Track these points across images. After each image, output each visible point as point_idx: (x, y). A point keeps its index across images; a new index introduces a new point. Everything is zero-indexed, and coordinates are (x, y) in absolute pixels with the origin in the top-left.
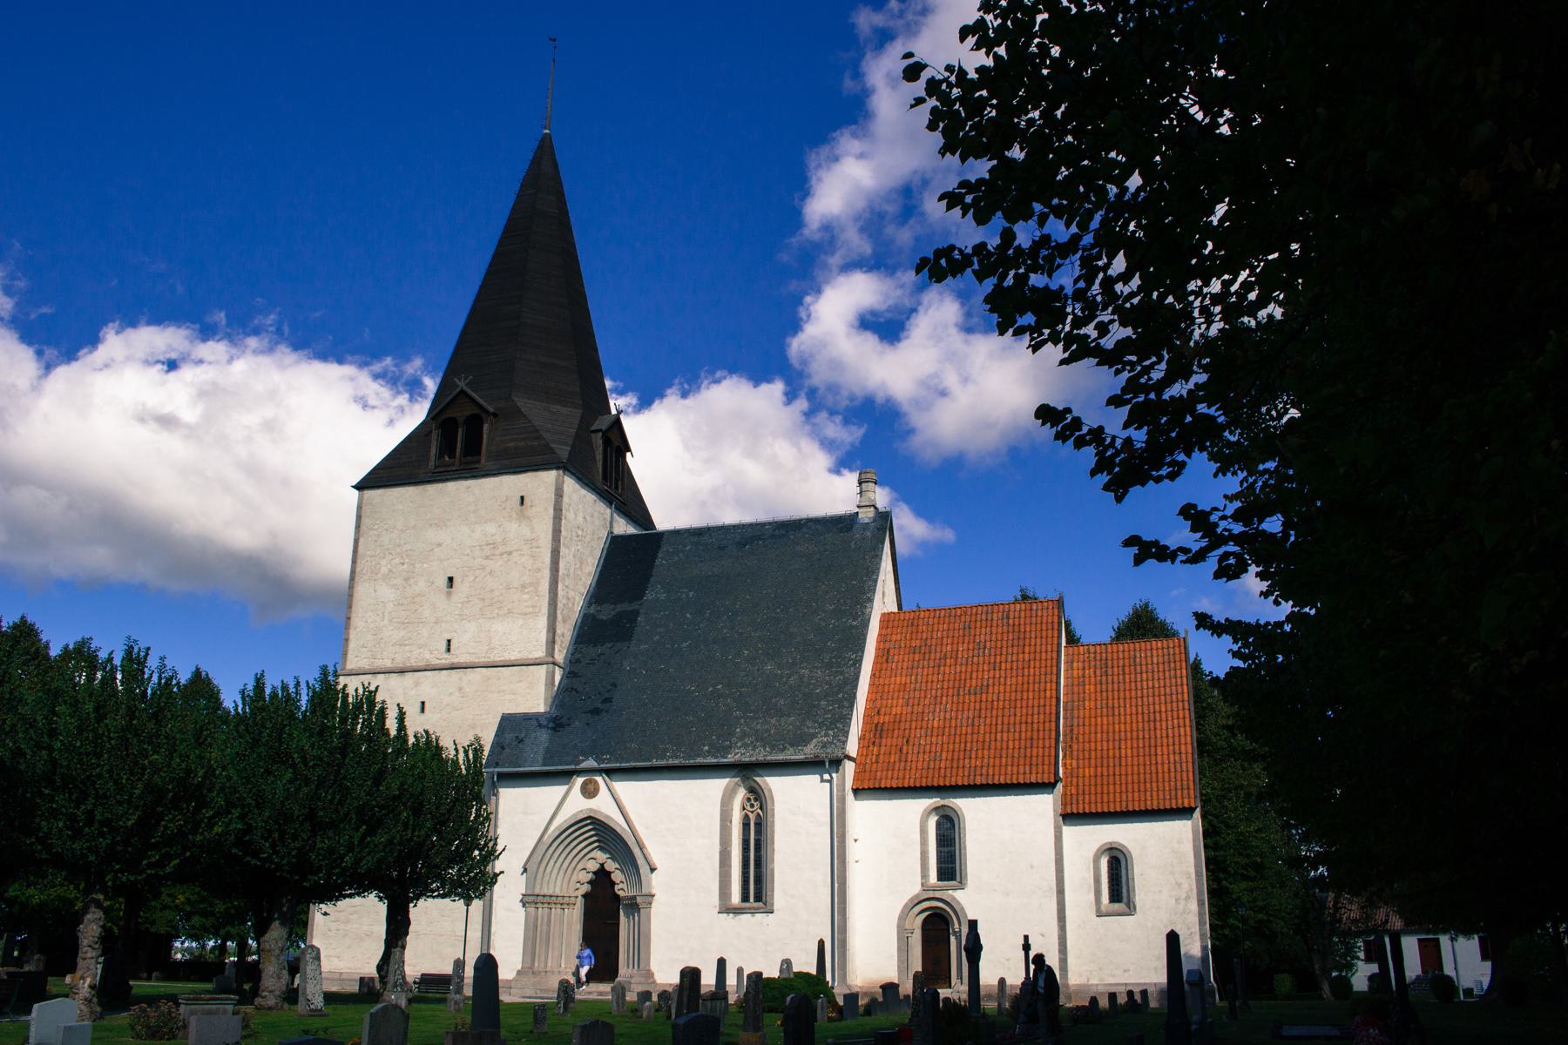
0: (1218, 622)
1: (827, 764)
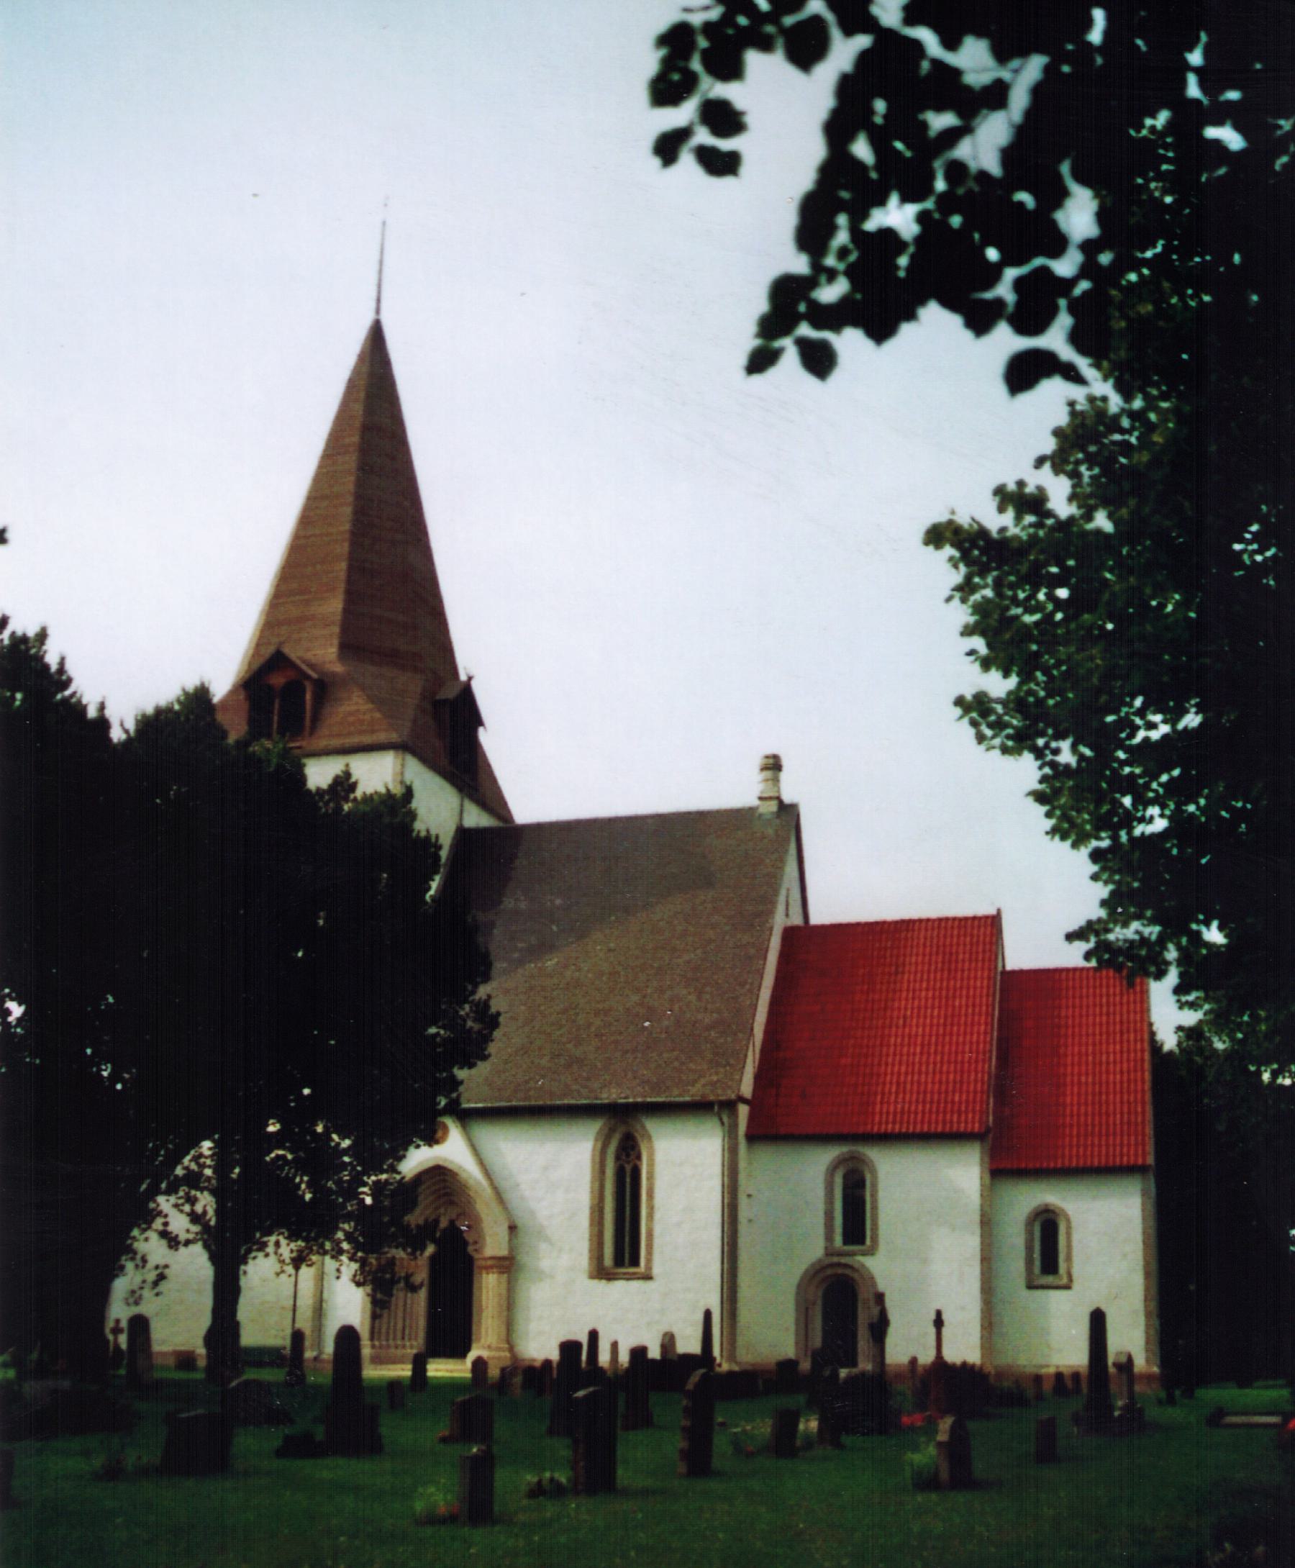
0: (1104, 903)
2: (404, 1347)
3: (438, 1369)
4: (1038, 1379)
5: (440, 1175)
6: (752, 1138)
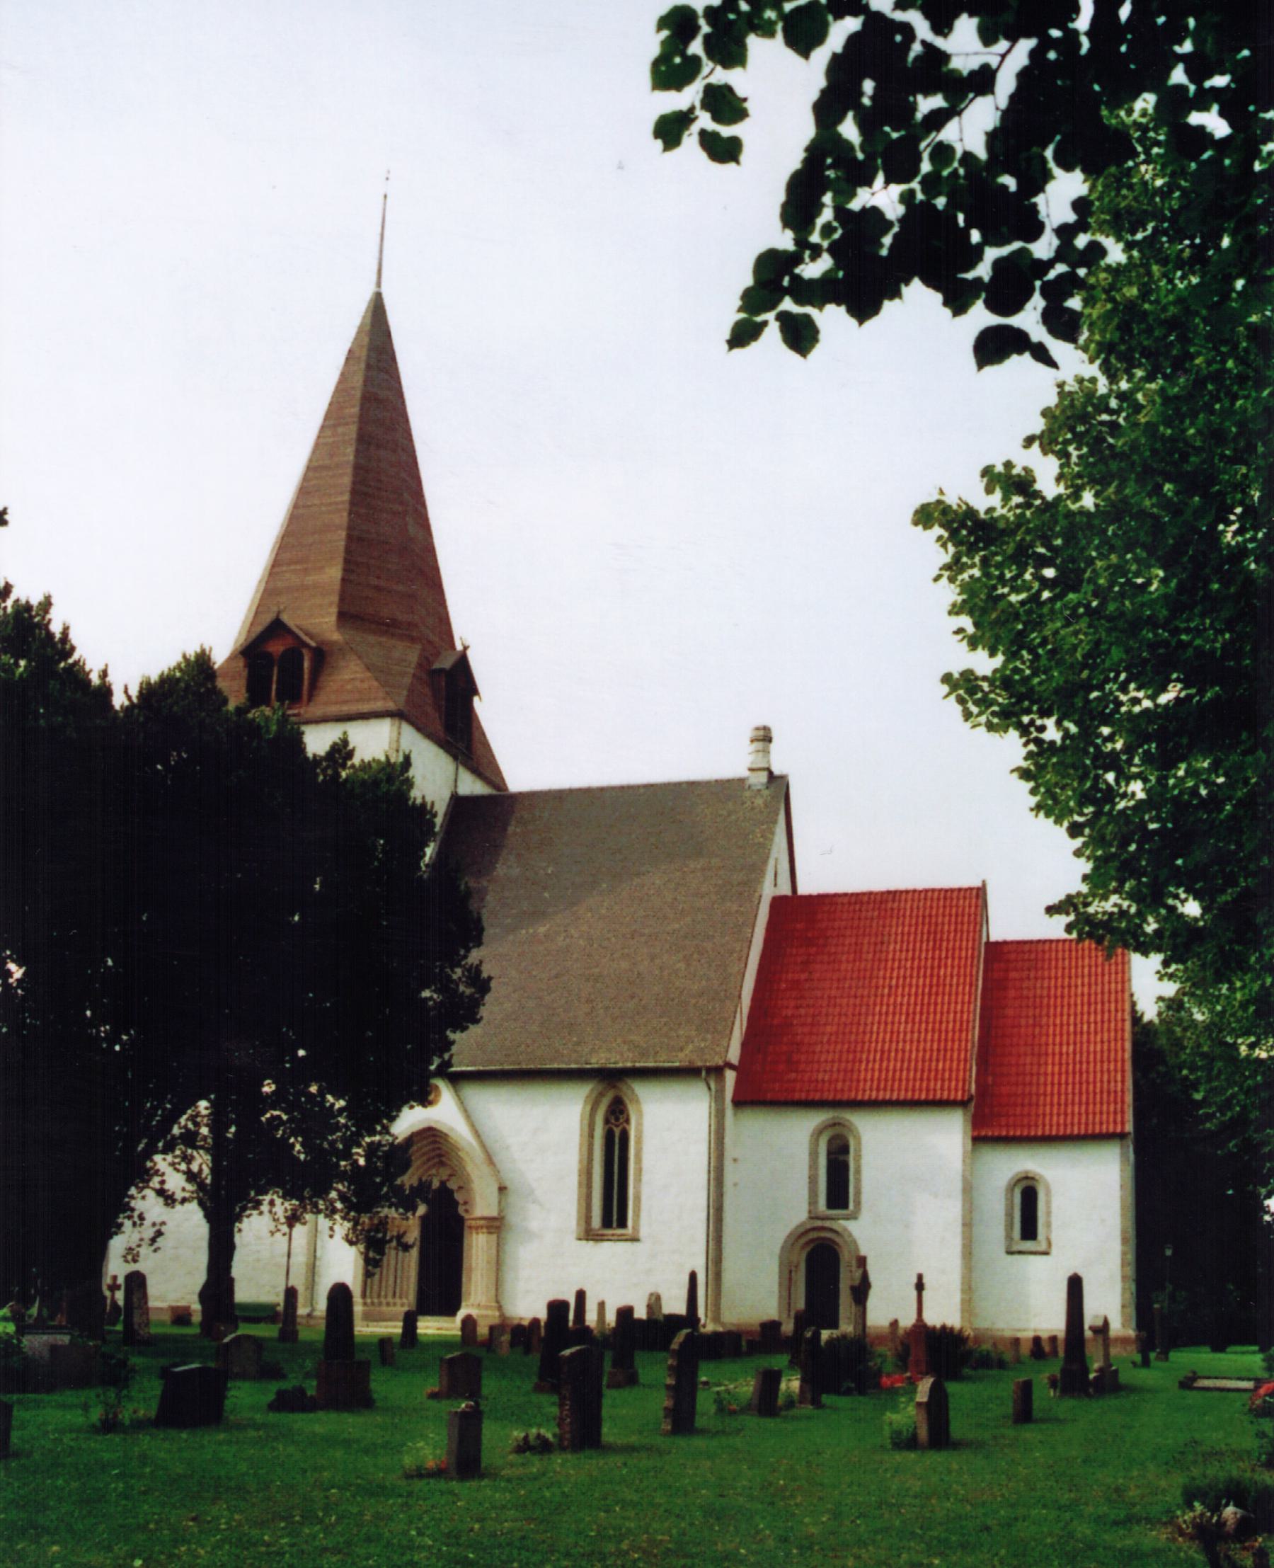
2: (395, 1304)
3: (429, 1327)
4: (1016, 1341)
5: (431, 1136)
6: (739, 1103)
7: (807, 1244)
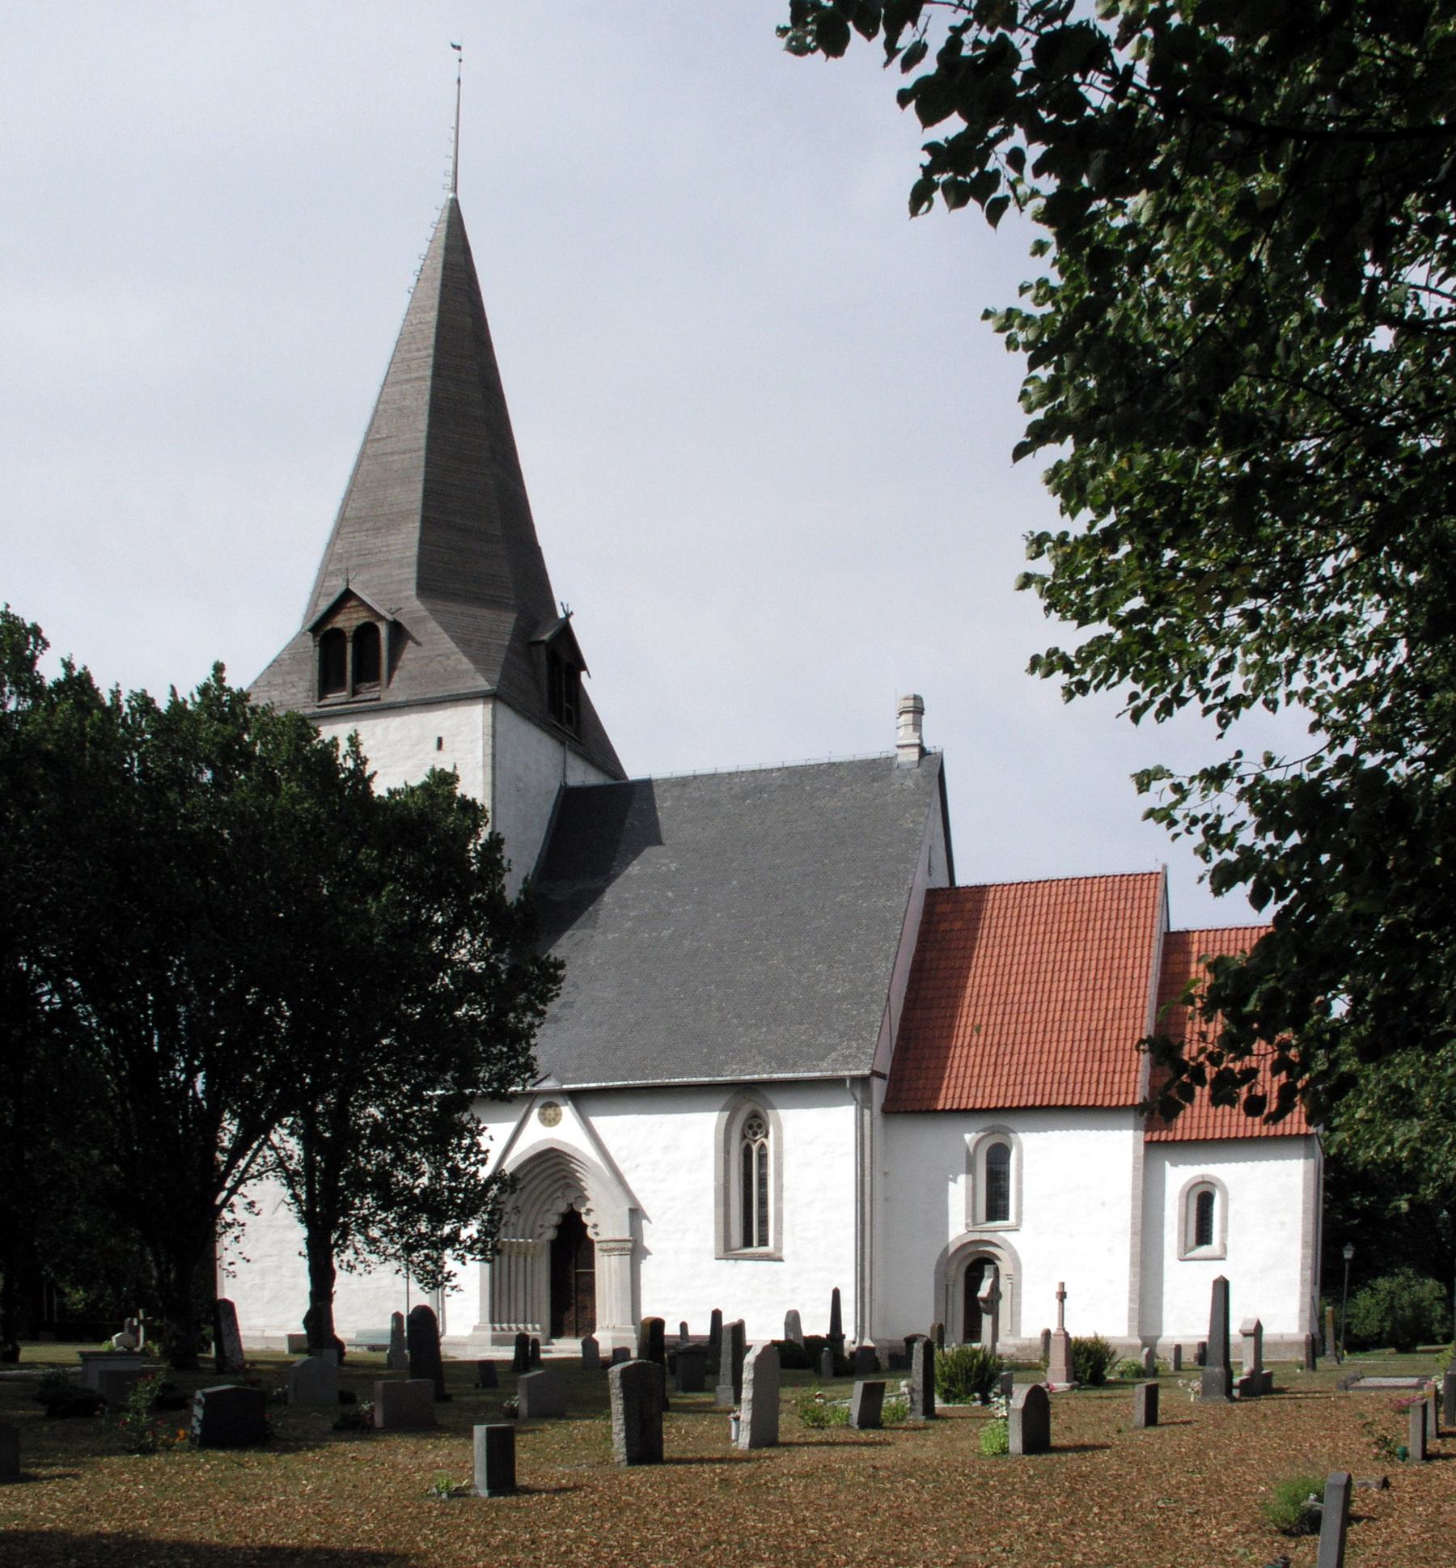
1: (848, 1082)
7: (966, 1257)
